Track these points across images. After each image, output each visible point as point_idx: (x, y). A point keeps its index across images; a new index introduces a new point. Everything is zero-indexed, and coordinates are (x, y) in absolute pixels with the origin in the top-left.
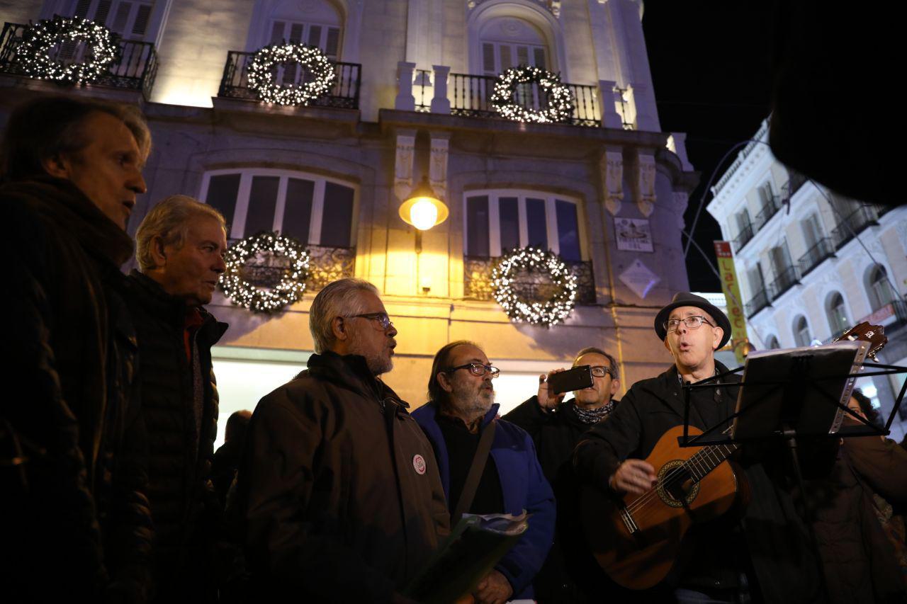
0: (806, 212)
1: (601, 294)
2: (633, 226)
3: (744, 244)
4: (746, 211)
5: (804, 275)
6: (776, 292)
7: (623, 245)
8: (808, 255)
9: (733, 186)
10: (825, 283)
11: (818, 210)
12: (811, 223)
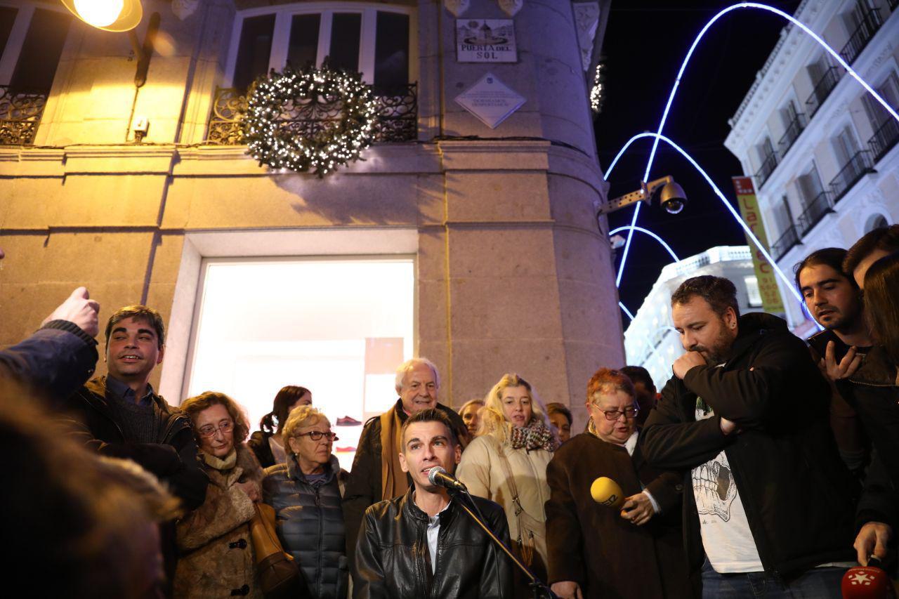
0: (836, 127)
1: (425, 127)
2: (486, 28)
3: (767, 177)
4: (768, 140)
5: (836, 201)
6: (806, 226)
7: (465, 55)
8: (842, 175)
9: (751, 113)
10: (864, 207)
11: (851, 121)
12: (843, 138)
